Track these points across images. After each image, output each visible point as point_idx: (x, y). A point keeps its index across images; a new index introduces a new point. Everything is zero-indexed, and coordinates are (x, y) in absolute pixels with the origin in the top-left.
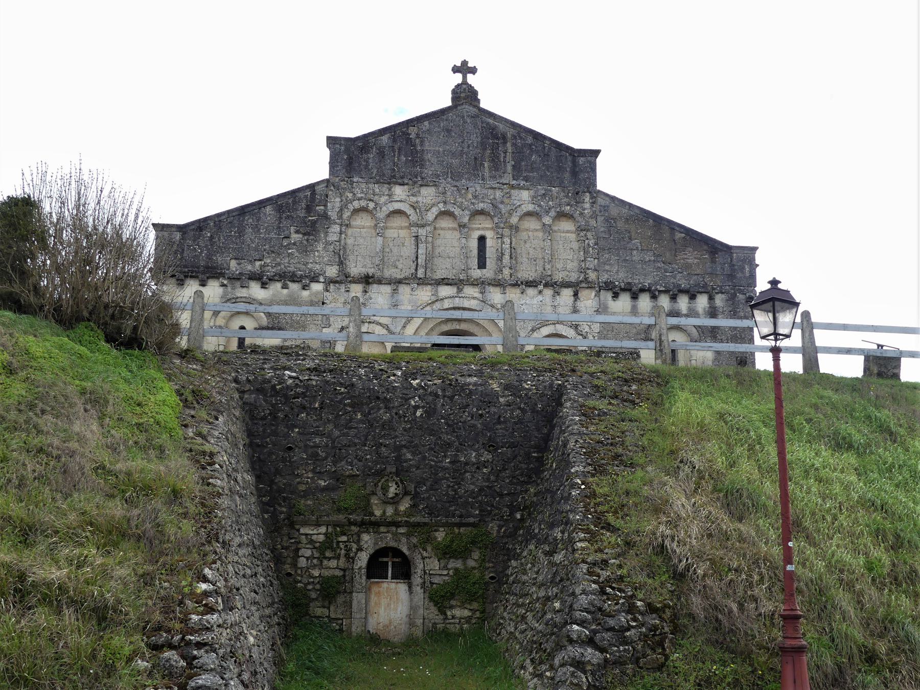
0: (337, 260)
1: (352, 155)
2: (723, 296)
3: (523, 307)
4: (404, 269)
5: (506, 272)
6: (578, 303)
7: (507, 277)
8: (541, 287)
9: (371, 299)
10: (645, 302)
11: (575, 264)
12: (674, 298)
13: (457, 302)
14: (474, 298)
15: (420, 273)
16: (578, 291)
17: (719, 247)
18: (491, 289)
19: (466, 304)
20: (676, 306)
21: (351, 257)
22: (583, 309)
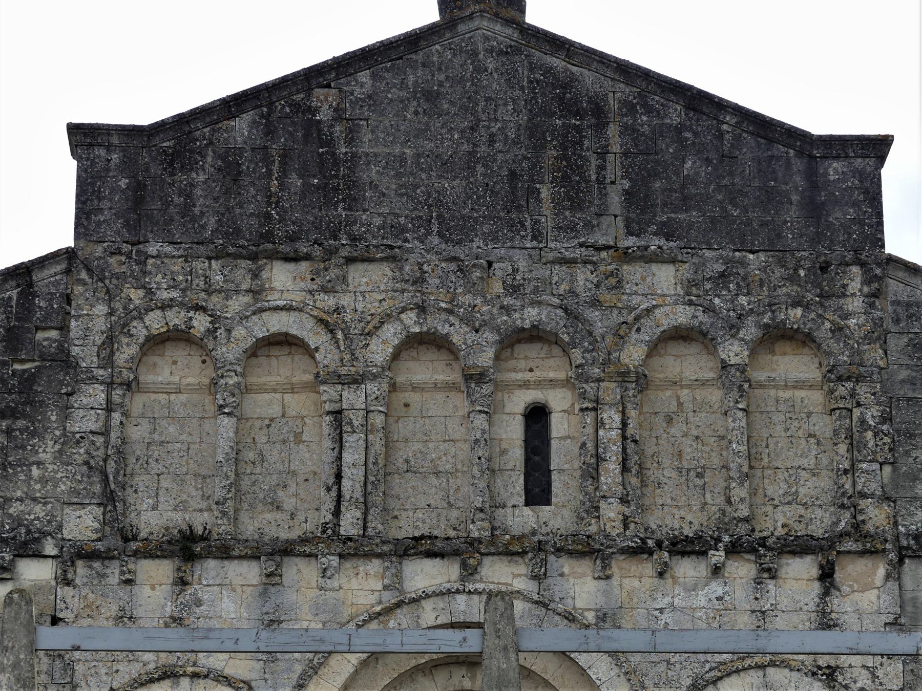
0: (97, 488)
4: (304, 511)
5: (611, 511)
6: (835, 602)
7: (614, 528)
8: (718, 556)
9: (199, 603)
11: (825, 482)
15: (349, 524)
18: (566, 565)
21: (141, 481)
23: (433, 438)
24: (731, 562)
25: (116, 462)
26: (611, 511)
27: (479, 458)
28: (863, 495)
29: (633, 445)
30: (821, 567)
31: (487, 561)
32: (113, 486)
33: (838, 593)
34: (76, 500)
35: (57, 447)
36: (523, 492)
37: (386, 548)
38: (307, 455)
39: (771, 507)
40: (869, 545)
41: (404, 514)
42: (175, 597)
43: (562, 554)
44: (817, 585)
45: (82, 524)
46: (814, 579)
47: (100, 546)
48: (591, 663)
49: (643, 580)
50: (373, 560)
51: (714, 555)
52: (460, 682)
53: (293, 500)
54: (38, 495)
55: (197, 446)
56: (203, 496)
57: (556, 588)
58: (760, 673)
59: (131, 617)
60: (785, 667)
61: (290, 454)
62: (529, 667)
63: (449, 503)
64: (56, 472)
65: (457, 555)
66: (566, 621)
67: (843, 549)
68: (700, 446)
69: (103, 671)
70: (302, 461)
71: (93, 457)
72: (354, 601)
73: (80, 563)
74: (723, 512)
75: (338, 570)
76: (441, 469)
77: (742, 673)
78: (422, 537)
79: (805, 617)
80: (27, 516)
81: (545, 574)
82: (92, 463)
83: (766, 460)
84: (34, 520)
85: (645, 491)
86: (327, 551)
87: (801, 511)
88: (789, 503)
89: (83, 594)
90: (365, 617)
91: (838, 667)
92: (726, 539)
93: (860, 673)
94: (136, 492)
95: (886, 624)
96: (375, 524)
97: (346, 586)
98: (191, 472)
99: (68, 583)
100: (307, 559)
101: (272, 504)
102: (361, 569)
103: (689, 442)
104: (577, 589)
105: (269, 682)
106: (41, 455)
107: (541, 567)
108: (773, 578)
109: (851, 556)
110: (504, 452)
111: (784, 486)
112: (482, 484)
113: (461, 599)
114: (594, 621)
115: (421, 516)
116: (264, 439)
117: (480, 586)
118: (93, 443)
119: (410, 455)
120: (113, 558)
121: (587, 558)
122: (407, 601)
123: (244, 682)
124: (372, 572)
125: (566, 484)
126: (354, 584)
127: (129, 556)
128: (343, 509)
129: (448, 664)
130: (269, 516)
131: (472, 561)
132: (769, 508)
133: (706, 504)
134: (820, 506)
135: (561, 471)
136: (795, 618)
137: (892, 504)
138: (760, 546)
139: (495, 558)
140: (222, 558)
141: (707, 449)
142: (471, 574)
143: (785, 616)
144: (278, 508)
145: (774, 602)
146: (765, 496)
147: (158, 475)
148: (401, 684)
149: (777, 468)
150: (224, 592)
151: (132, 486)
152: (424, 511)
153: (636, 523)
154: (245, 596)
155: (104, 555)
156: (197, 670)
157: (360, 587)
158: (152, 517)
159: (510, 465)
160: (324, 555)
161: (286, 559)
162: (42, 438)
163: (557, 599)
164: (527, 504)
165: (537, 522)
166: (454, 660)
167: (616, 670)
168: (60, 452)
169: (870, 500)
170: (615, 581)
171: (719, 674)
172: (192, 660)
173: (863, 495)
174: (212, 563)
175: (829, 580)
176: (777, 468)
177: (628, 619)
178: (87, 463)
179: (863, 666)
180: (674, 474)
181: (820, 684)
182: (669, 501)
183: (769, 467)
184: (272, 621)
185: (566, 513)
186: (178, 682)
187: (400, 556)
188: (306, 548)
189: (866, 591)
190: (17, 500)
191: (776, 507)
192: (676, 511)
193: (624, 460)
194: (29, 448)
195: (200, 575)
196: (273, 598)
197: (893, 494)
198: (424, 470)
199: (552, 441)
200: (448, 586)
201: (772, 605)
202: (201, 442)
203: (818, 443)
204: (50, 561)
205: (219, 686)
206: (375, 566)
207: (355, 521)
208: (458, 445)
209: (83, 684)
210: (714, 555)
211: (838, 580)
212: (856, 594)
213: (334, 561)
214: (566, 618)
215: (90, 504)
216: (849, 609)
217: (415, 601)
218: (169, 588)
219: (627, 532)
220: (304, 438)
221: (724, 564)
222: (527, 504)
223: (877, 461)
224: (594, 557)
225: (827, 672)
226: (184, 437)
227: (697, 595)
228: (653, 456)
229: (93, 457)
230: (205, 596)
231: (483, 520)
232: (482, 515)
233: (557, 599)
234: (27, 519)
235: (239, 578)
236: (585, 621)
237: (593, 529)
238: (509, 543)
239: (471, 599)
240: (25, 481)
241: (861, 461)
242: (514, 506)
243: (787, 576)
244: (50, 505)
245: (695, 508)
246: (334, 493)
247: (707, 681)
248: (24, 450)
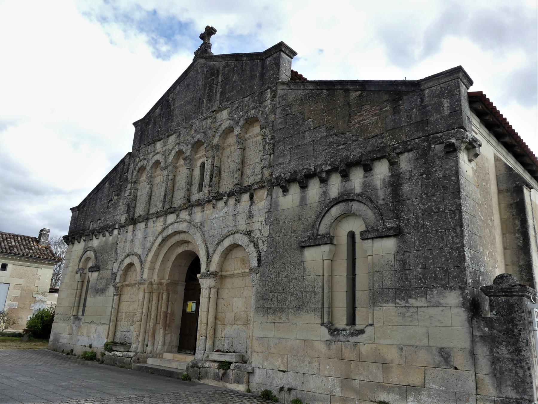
1: (148, 129)
2: (411, 155)
3: (214, 222)
8: (225, 198)
10: (314, 189)
12: (345, 176)
17: (404, 89)
20: (348, 185)
111: (251, 170)
170: (205, 212)
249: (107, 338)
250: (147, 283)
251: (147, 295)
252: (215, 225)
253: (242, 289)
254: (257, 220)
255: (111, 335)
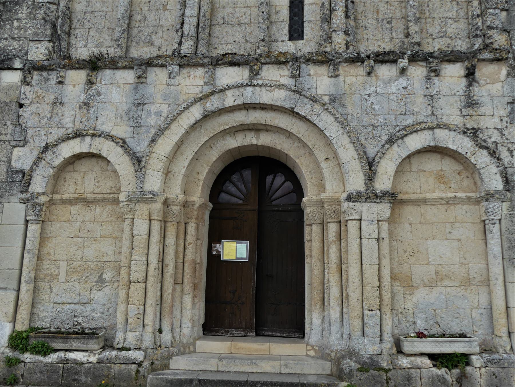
0: (49, 32)
3: (372, 99)
4: (165, 43)
5: (339, 39)
6: (476, 90)
7: (341, 48)
8: (404, 62)
9: (99, 94)
11: (462, 25)
13: (250, 95)
14: (280, 86)
15: (187, 48)
16: (474, 67)
18: (312, 69)
19: (266, 97)
21: (79, 32)
22: (485, 100)
23: (238, 6)
24: (411, 67)
25: (62, 19)
26: (339, 39)
27: (263, 12)
28: (490, 28)
29: (351, 4)
30: (467, 68)
31: (265, 67)
32: (59, 32)
33: (477, 85)
34: (36, 39)
35: (29, 10)
36: (288, 33)
37: (206, 60)
38: (169, 17)
39: (431, 40)
40: (498, 55)
41: (221, 46)
42: (86, 91)
43: (310, 63)
44: (464, 80)
45: (39, 52)
46: (462, 77)
47: (46, 63)
48: (326, 127)
49: (358, 78)
50: (199, 68)
51: (402, 62)
52: (251, 140)
53: (160, 40)
54: (16, 36)
55: (111, 13)
56: (112, 39)
57: (306, 83)
58: (431, 132)
59: (61, 103)
60: (446, 129)
61: (160, 16)
62: (289, 130)
63: (246, 40)
64: (26, 23)
65: (247, 64)
66: (311, 102)
67: (481, 57)
68: (389, 7)
69: (43, 133)
70: (166, 20)
71: (48, 16)
72: (187, 92)
73: (36, 73)
74: (403, 42)
75: (178, 74)
76: (242, 22)
77: (419, 133)
78: (226, 54)
79: (458, 99)
80: (9, 48)
81: (299, 75)
82: (47, 19)
83: (427, 14)
84: (12, 49)
85: (358, 31)
86: (171, 62)
87: (449, 41)
88: (442, 37)
89: (36, 90)
90: (192, 100)
91: (479, 129)
92: (409, 53)
93: (493, 132)
94: (76, 37)
95: (508, 103)
96: (202, 49)
97: (182, 82)
98: (106, 27)
99: (28, 84)
100: (161, 68)
101: (149, 42)
102: (192, 73)
103: (383, 5)
104: (318, 83)
105: (136, 139)
106: (19, 15)
107: (297, 70)
108: (437, 76)
109: (485, 63)
110: (277, 12)
111: (438, 28)
112: (264, 26)
113: (249, 89)
114: (328, 102)
115: (230, 47)
116: (147, 9)
117: (260, 82)
118: (49, 8)
119: (226, 15)
120: (53, 70)
121: (325, 65)
122: (217, 91)
123: (121, 139)
124: (198, 75)
125: (312, 28)
126: (188, 82)
127: (62, 68)
128: (183, 40)
129: (244, 130)
130: (146, 49)
131: (255, 67)
132: (430, 40)
133: (393, 38)
134: (460, 38)
135: (309, 22)
136: (452, 100)
137: (507, 34)
138: (429, 57)
139: (270, 66)
140: (114, 69)
141: (393, 8)
142: (256, 75)
143: (445, 98)
144: (152, 44)
145: (438, 90)
146: (428, 33)
147: (89, 29)
148: (217, 141)
149: (434, 18)
150: (113, 88)
151: (74, 35)
152: (232, 44)
153: (353, 46)
154: (125, 90)
155: (48, 68)
156: (95, 132)
157: (191, 84)
158: (82, 51)
159: (281, 19)
160: (170, 65)
161: (149, 69)
162: (21, 6)
163: (306, 89)
164: (290, 40)
165: (296, 49)
166: (246, 127)
167: (342, 131)
168: (30, 13)
169: (495, 30)
170: (341, 78)
171: (406, 133)
172: (93, 126)
173: (490, 28)
174: (108, 72)
175: (471, 77)
176: (434, 18)
177: (349, 100)
178: (44, 19)
179: (495, 128)
180: (374, 22)
181: (468, 139)
182: (371, 37)
183: (429, 18)
184: (139, 104)
185: (312, 44)
186: (84, 139)
187: (214, 66)
188: (159, 61)
189: (493, 80)
190: (5, 39)
191: (434, 39)
192: (375, 42)
193: (347, 12)
194: (14, 11)
195: (101, 79)
196: (141, 91)
197: (508, 28)
198: (233, 22)
199: (305, 6)
200: (242, 82)
201: (437, 92)
202: (113, 11)
203: (458, 4)
204: (19, 71)
205: (107, 141)
206: (200, 71)
207: (190, 47)
208: (252, 9)
209: (31, 141)
210: (402, 62)
211: (477, 77)
212: (489, 85)
213: (176, 68)
214: (312, 100)
215: (44, 41)
216: (484, 94)
217: (222, 91)
218: (83, 86)
219: (348, 51)
220: (168, 8)
221: (407, 67)
222: (290, 40)
223: (499, 8)
224: (328, 65)
225: (473, 131)
226: (104, 9)
227: (391, 86)
228: (362, 12)
229: (48, 16)
230: (102, 90)
231: (264, 46)
232: (263, 43)
233: (306, 89)
234: (8, 49)
235: (123, 80)
236: (322, 102)
237: (328, 49)
238: (278, 56)
239: (255, 90)
240: (9, 29)
241: (488, 8)
242: (282, 41)
243: (445, 75)
244: (22, 41)
245: (386, 40)
246: (180, 33)
247: (398, 137)
248: (11, 13)
249: (14, 321)
250: (160, 200)
251: (156, 226)
252: (377, 107)
253: (448, 225)
254: (489, 112)
255: (23, 314)
